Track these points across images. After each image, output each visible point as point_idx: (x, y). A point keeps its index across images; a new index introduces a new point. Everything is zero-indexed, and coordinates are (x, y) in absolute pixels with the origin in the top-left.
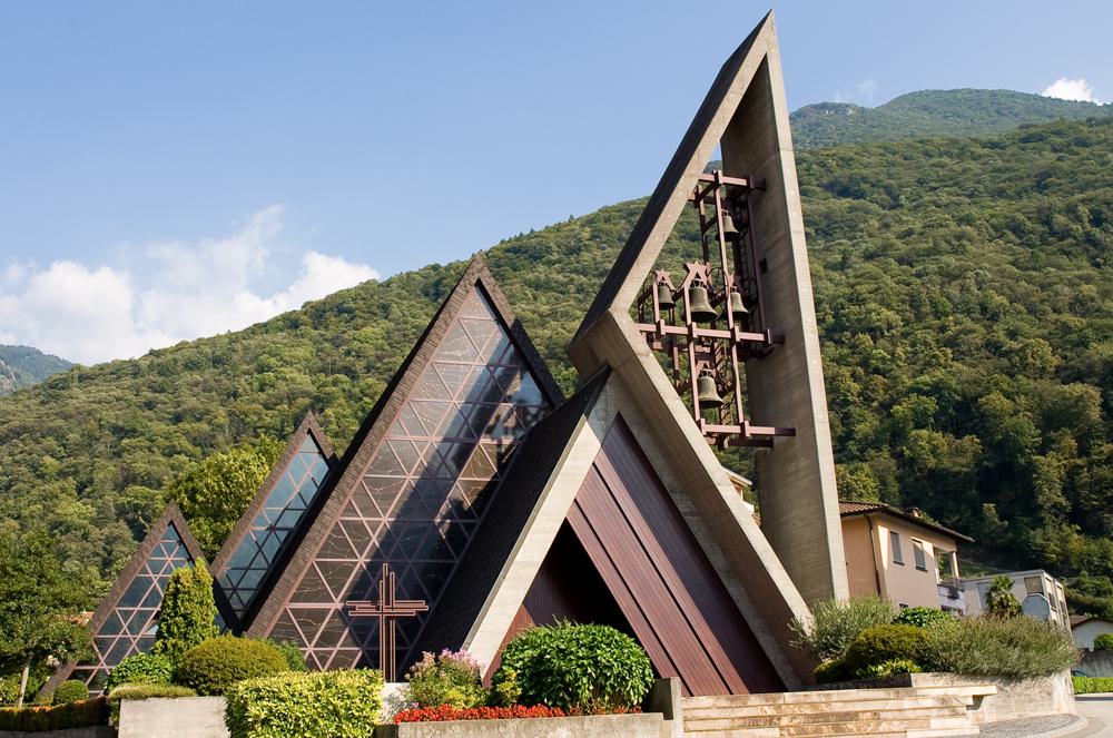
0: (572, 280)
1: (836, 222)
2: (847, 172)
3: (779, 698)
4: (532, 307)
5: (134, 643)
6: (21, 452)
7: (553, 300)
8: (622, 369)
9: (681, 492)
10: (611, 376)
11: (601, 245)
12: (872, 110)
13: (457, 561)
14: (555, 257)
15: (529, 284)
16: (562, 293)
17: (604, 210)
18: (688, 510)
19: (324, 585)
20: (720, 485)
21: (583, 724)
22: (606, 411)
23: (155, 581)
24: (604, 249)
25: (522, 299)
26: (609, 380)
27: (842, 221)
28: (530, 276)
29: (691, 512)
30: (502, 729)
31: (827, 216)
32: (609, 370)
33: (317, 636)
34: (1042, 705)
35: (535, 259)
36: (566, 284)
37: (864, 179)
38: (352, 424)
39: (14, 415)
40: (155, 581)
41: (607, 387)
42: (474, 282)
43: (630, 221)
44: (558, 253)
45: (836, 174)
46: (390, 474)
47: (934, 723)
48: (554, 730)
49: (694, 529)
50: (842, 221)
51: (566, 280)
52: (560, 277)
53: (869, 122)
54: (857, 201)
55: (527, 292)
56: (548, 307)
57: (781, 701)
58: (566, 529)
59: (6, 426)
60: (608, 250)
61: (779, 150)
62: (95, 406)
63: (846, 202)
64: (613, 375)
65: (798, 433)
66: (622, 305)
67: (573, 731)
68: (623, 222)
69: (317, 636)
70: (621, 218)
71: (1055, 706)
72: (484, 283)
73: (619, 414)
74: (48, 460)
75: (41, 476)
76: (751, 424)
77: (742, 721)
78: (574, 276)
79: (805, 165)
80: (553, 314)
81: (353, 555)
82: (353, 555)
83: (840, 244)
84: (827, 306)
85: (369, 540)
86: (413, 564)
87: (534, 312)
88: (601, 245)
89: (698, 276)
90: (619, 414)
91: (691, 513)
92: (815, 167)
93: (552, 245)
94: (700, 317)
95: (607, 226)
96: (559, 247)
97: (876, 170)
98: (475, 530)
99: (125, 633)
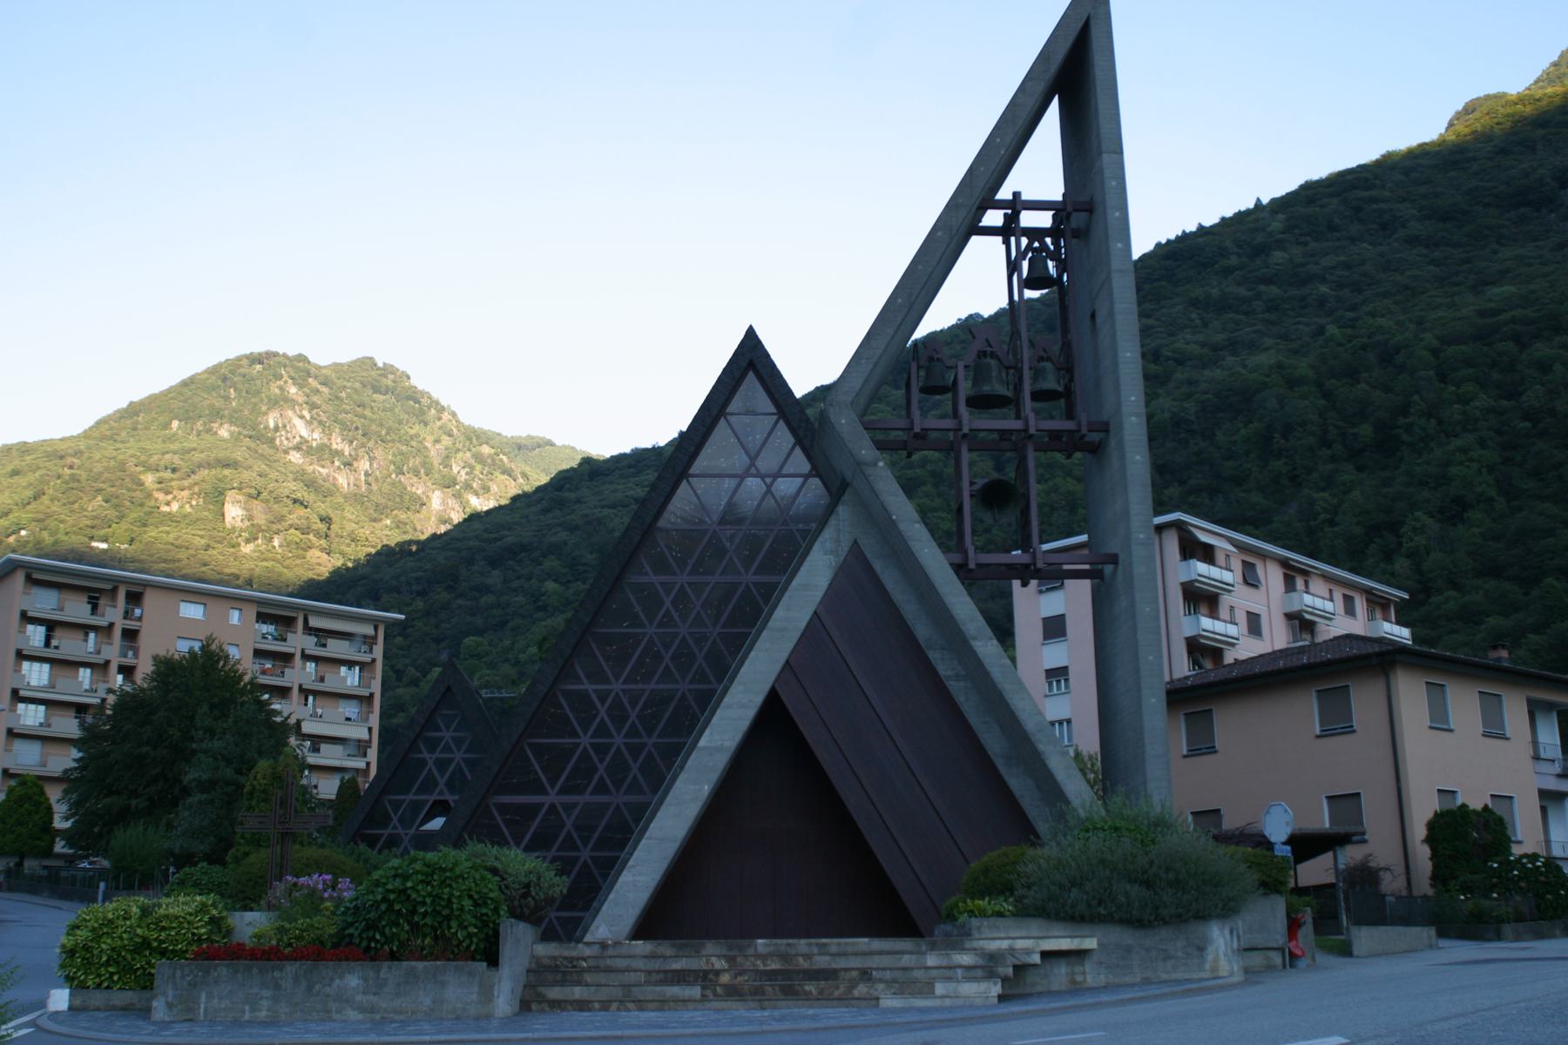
3: (749, 946)
4: (1200, 337)
5: (406, 839)
6: (519, 578)
10: (846, 494)
14: (1234, 261)
15: (1195, 303)
16: (1246, 314)
18: (950, 673)
19: (537, 773)
20: (975, 639)
21: (378, 972)
22: (838, 541)
23: (430, 763)
24: (1306, 244)
26: (843, 498)
29: (957, 676)
30: (277, 974)
32: (848, 484)
33: (528, 837)
34: (1186, 964)
38: (943, 519)
39: (510, 529)
40: (430, 763)
44: (1239, 255)
46: (627, 627)
47: (940, 989)
48: (341, 977)
49: (960, 699)
51: (1249, 294)
52: (1242, 291)
55: (1194, 316)
57: (751, 951)
59: (499, 543)
62: (607, 512)
64: (849, 491)
67: (365, 980)
68: (1335, 201)
69: (528, 837)
71: (1207, 966)
73: (856, 542)
74: (551, 586)
75: (543, 608)
77: (661, 976)
78: (1262, 288)
80: (1233, 346)
81: (574, 734)
82: (574, 734)
85: (595, 716)
86: (654, 744)
87: (1203, 345)
90: (856, 542)
91: (957, 677)
93: (1228, 243)
94: (980, 402)
99: (395, 828)
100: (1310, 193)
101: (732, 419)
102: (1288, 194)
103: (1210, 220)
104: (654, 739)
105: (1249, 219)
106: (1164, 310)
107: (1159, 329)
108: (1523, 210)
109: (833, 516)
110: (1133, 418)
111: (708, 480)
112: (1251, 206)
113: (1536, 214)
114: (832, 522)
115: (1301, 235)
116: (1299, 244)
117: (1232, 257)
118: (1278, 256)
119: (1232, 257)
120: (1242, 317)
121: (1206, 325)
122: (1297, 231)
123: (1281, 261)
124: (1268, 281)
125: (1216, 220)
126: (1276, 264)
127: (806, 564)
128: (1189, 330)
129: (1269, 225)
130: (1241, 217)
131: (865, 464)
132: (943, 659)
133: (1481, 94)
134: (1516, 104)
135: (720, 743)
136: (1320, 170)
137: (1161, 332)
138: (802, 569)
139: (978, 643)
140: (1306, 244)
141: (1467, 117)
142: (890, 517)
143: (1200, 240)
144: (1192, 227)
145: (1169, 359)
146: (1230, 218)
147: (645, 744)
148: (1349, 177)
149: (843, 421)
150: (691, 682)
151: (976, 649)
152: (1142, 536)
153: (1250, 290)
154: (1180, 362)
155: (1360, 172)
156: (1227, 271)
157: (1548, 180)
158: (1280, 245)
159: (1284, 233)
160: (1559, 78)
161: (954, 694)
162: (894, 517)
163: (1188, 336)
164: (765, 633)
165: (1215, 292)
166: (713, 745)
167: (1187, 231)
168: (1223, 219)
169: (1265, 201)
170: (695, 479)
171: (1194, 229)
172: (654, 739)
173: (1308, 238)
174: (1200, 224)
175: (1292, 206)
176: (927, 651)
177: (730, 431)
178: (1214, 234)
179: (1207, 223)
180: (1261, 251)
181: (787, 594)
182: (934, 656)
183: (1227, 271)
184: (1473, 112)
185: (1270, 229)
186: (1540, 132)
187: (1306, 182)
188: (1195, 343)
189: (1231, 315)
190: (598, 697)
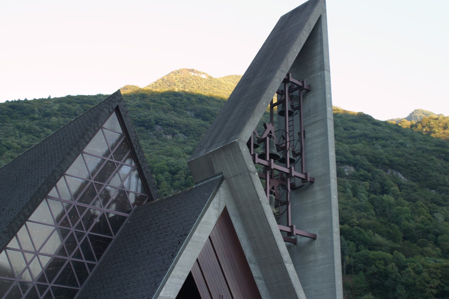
0: (44, 131)
1: (191, 130)
2: (200, 106)
7: (31, 140)
8: (233, 179)
9: (255, 264)
11: (64, 116)
12: (215, 79)
13: (80, 289)
14: (36, 116)
15: (18, 127)
16: (37, 137)
17: (69, 97)
20: (286, 262)
22: (219, 204)
24: (65, 118)
25: (13, 135)
26: (222, 185)
27: (194, 130)
28: (20, 124)
29: (259, 277)
31: (186, 126)
35: (25, 114)
36: (40, 132)
37: (208, 111)
41: (221, 189)
42: (115, 107)
43: (82, 106)
44: (39, 114)
45: (194, 106)
50: (194, 130)
51: (40, 130)
52: (38, 128)
53: (213, 84)
54: (203, 122)
55: (17, 132)
56: (27, 143)
58: (190, 279)
60: (67, 119)
61: (324, 70)
63: (199, 121)
64: (224, 181)
65: (318, 237)
66: (244, 139)
68: (78, 105)
70: (77, 103)
72: (121, 110)
76: (297, 228)
78: (46, 129)
79: (180, 98)
83: (192, 142)
84: (183, 172)
86: (52, 287)
88: (64, 116)
89: (270, 132)
92: (185, 100)
93: (36, 109)
95: (68, 106)
96: (40, 111)
97: (215, 108)
98: (94, 269)
100: (69, 100)
101: (105, 131)
102: (61, 98)
103: (30, 98)
104: (52, 284)
105: (45, 102)
106: (5, 127)
107: (2, 133)
108: (142, 128)
109: (218, 192)
110: (333, 180)
111: (91, 157)
112: (47, 98)
113: (146, 130)
114: (218, 195)
115: (64, 114)
116: (62, 117)
117: (36, 114)
118: (54, 119)
119: (36, 114)
120: (36, 138)
121: (21, 137)
122: (63, 112)
123: (54, 121)
124: (48, 127)
125: (32, 99)
126: (53, 122)
127: (206, 214)
128: (14, 137)
129: (53, 107)
130: (42, 101)
131: (251, 172)
132: (254, 268)
133: (131, 85)
134: (146, 91)
135: (169, 295)
136: (74, 93)
137: (2, 135)
138: (206, 214)
139: (287, 265)
140: (65, 118)
141: (124, 90)
142: (259, 199)
143: (25, 104)
144: (23, 99)
145: (4, 146)
146: (37, 100)
147: (47, 286)
148: (85, 98)
149: (244, 150)
150: (73, 257)
151: (286, 267)
152: (336, 230)
153: (40, 128)
154: (8, 148)
155: (89, 98)
156: (33, 119)
157: (153, 120)
158: (56, 115)
159: (58, 111)
160: (156, 87)
161: (258, 285)
162: (260, 199)
163: (13, 139)
164: (190, 242)
165: (27, 125)
166: (166, 296)
167: (21, 99)
168: (35, 99)
169: (52, 97)
170: (86, 155)
171: (23, 100)
172: (52, 284)
173: (66, 116)
174: (19, 99)
175: (62, 102)
176: (249, 263)
177: (103, 136)
178: (31, 104)
179: (28, 99)
180: (47, 115)
181: (200, 225)
182: (252, 266)
183: (33, 119)
184: (126, 89)
185: (53, 108)
186: (152, 103)
187: (69, 95)
188: (15, 142)
189: (32, 136)
190: (77, 258)
